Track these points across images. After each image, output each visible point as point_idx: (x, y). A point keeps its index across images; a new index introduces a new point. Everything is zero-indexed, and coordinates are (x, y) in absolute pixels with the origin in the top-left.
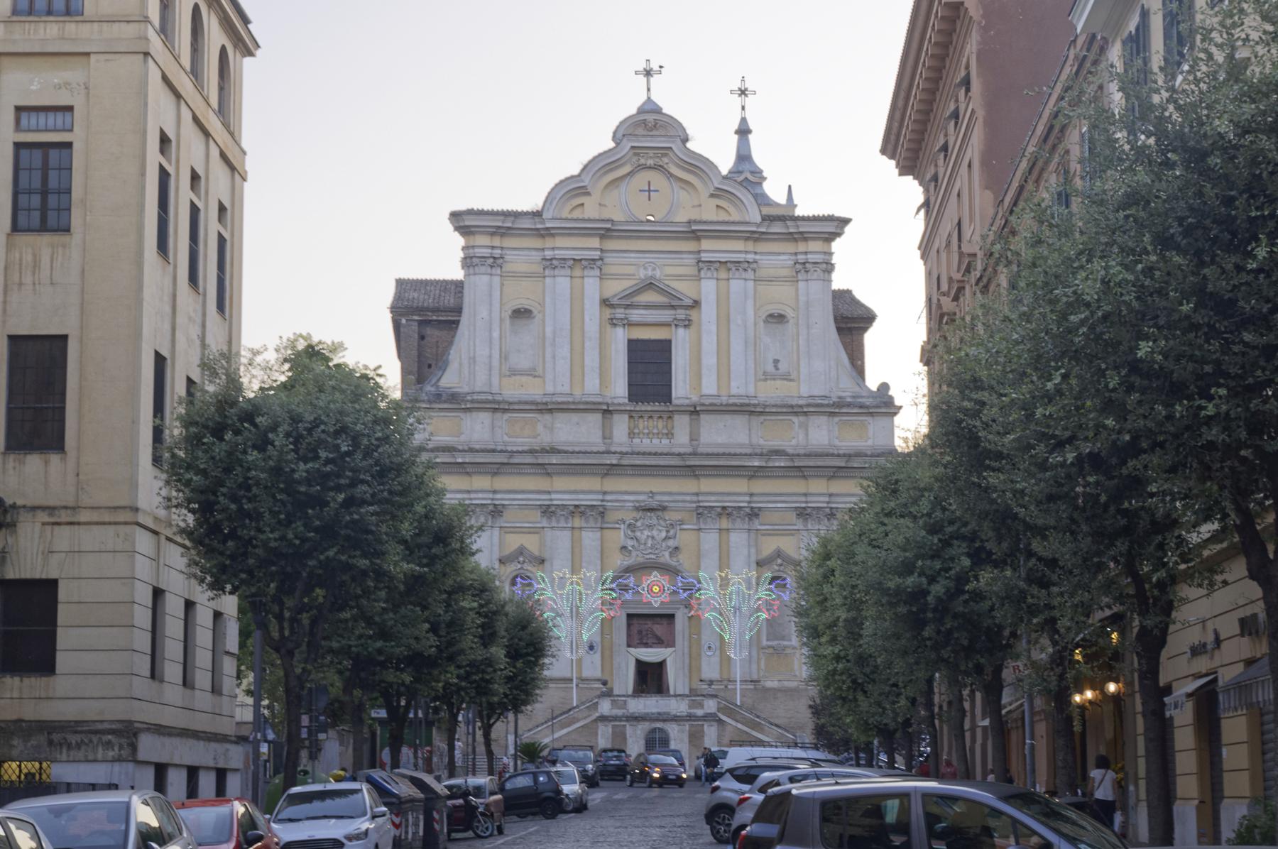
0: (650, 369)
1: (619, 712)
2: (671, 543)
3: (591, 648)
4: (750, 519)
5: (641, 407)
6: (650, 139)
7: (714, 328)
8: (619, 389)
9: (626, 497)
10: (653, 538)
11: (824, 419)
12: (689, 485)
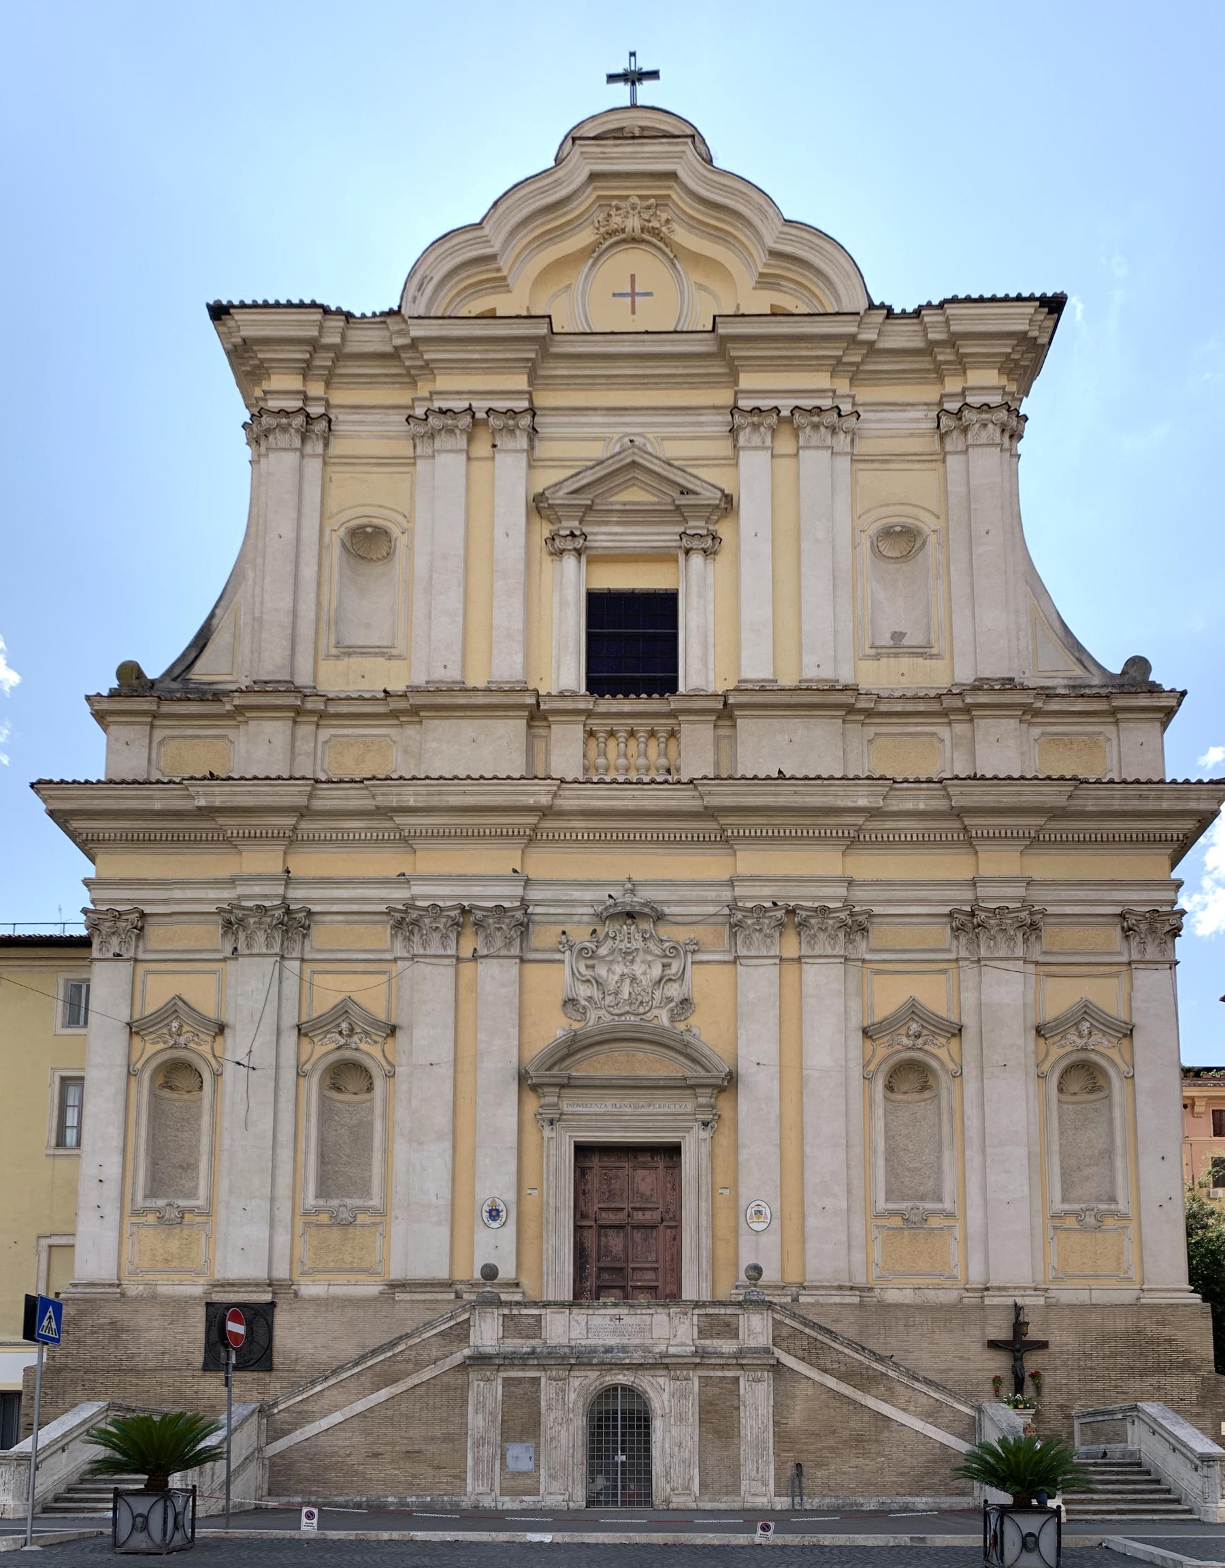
0: (632, 643)
1: (524, 1345)
2: (674, 990)
3: (494, 1214)
4: (850, 941)
5: (608, 704)
6: (634, 172)
7: (766, 548)
8: (565, 669)
9: (577, 894)
10: (634, 979)
11: (1009, 725)
12: (708, 866)
